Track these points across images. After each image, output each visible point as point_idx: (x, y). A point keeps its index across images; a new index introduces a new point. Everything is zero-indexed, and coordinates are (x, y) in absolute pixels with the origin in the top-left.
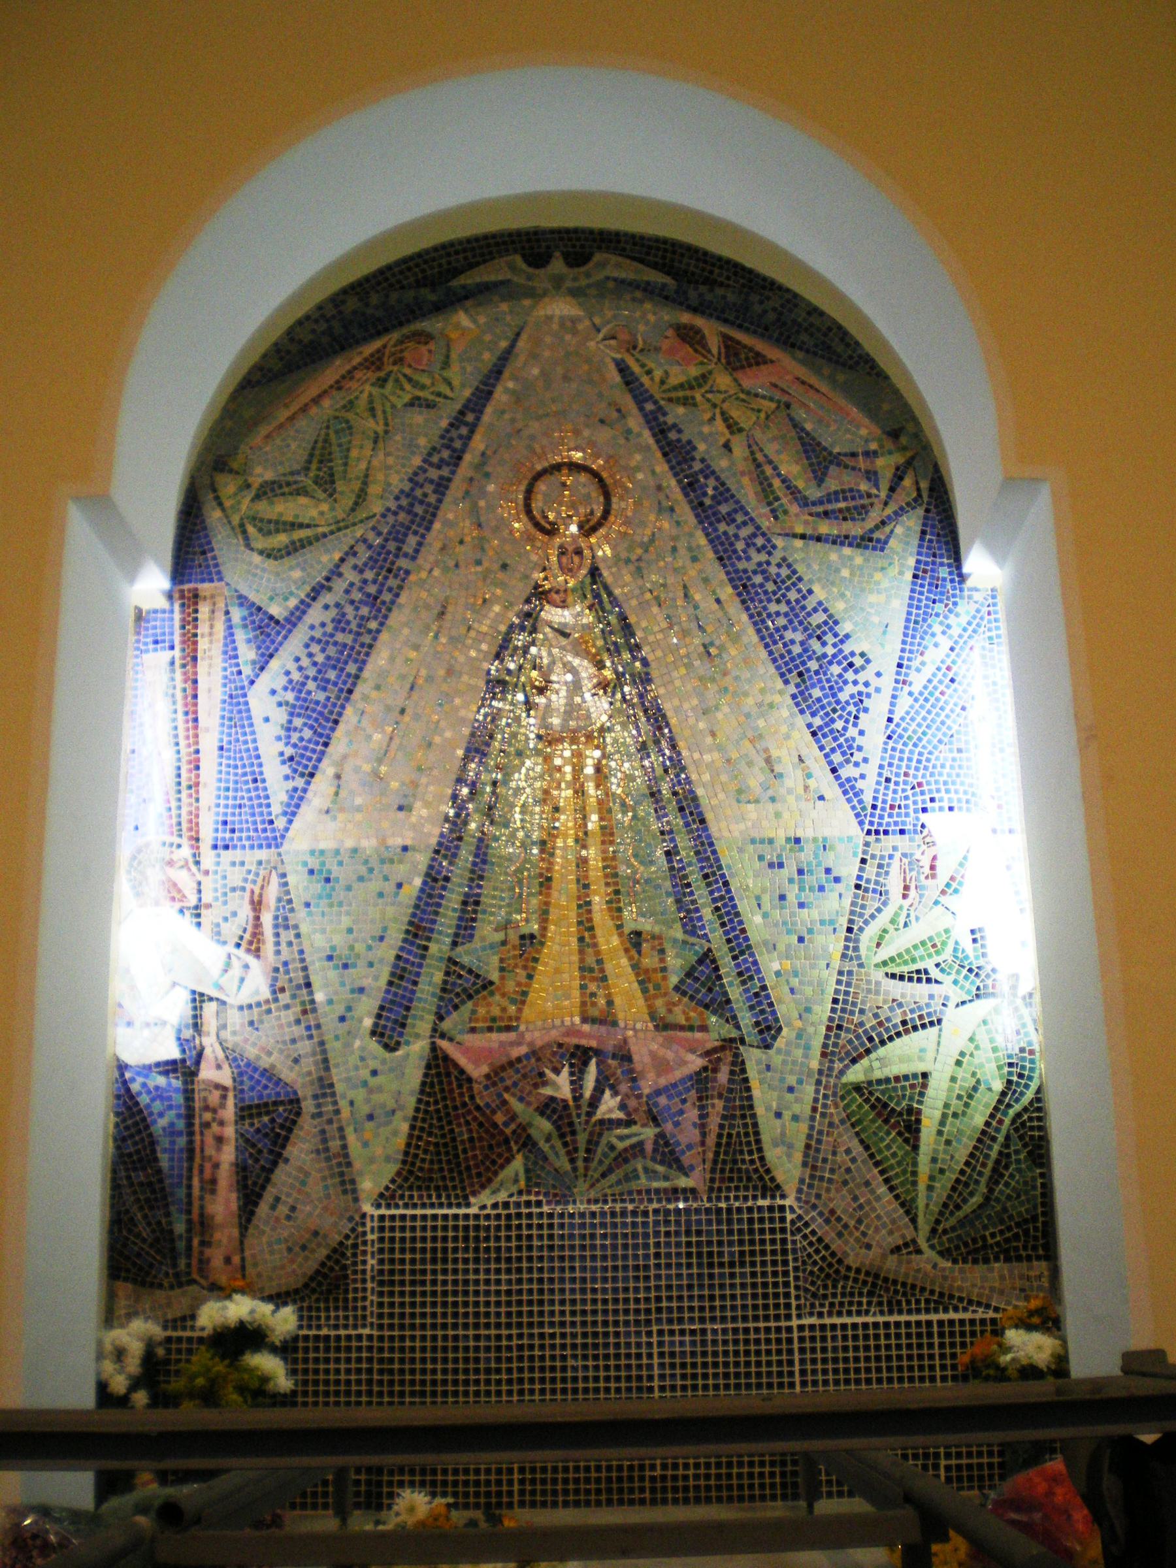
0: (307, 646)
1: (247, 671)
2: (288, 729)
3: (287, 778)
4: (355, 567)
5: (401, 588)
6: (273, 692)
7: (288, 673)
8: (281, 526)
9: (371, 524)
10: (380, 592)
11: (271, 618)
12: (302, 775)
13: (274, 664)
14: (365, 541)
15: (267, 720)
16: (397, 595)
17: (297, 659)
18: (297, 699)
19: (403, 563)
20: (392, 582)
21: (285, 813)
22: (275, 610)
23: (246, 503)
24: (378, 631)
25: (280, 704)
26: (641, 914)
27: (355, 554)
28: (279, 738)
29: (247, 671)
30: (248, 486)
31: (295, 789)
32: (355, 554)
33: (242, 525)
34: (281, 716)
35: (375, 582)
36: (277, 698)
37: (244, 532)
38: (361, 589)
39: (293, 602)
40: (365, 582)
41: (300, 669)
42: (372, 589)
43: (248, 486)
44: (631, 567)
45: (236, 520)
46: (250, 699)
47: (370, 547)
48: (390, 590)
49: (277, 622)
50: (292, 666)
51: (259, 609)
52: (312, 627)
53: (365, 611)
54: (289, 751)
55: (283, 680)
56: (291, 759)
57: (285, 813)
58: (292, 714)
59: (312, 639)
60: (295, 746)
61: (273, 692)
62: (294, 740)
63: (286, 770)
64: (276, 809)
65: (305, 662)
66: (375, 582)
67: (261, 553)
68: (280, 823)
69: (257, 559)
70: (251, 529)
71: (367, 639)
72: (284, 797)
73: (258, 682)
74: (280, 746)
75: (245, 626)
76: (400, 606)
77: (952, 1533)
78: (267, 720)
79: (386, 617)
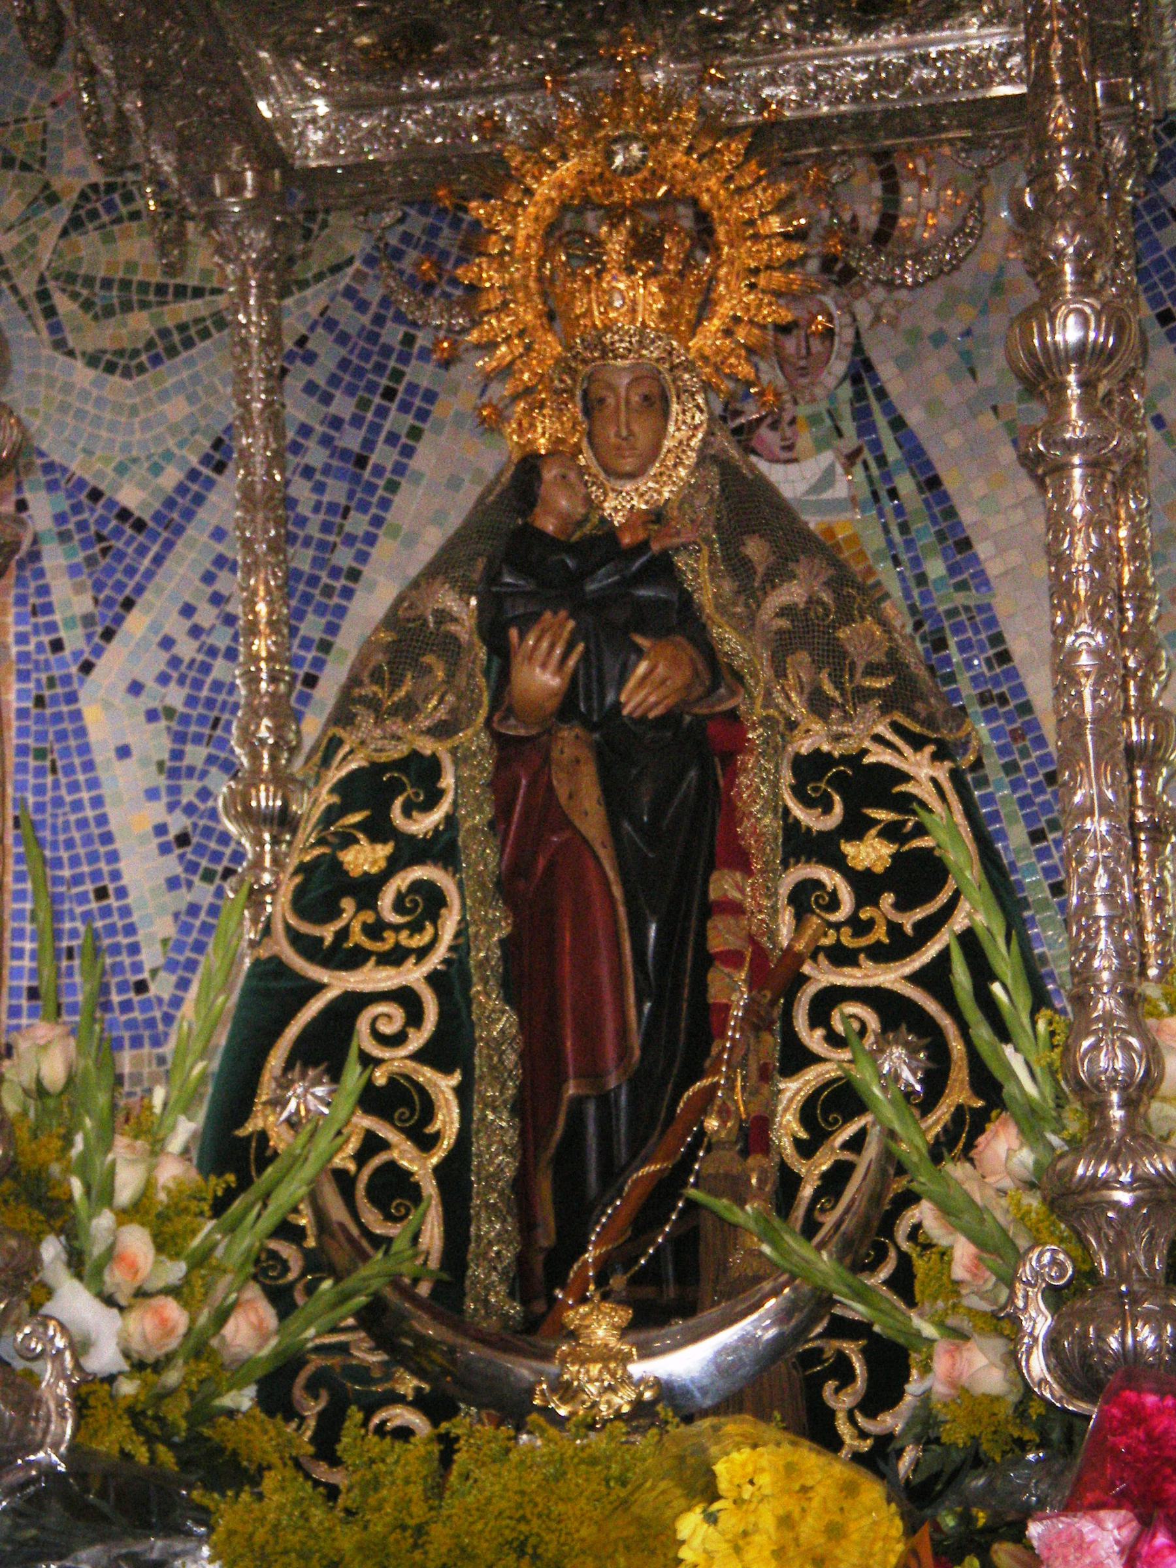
0: (209, 578)
1: (74, 639)
2: (174, 773)
3: (173, 883)
4: (311, 388)
5: (415, 433)
6: (136, 688)
7: (167, 643)
8: (128, 294)
9: (345, 279)
10: (369, 444)
11: (124, 514)
12: (208, 876)
13: (136, 624)
14: (330, 325)
15: (124, 752)
16: (408, 452)
17: (188, 611)
18: (191, 701)
19: (421, 374)
20: (397, 421)
21: (171, 966)
22: (130, 496)
23: (50, 238)
24: (371, 539)
25: (152, 716)
26: (1095, 652)
27: (310, 358)
28: (152, 794)
29: (74, 639)
30: (53, 199)
31: (193, 909)
32: (310, 358)
33: (43, 295)
34: (155, 742)
35: (357, 421)
36: (145, 702)
37: (50, 312)
38: (326, 441)
39: (171, 477)
40: (336, 423)
41: (196, 631)
42: (352, 440)
43: (53, 199)
44: (949, 355)
45: (28, 289)
46: (82, 705)
47: (343, 339)
48: (392, 439)
49: (139, 525)
50: (177, 627)
51: (96, 495)
52: (219, 534)
53: (336, 491)
54: (178, 823)
55: (159, 661)
56: (183, 839)
57: (171, 966)
58: (180, 738)
59: (221, 561)
60: (190, 809)
61: (136, 688)
62: (187, 797)
63: (172, 865)
64: (151, 956)
65: (207, 615)
66: (357, 421)
67: (93, 361)
68: (162, 987)
69: (83, 375)
70: (63, 304)
71: (344, 558)
72: (166, 927)
73: (102, 665)
74: (156, 812)
75: (64, 537)
76: (417, 478)
77: (249, 1128)
78: (124, 752)
79: (385, 504)
